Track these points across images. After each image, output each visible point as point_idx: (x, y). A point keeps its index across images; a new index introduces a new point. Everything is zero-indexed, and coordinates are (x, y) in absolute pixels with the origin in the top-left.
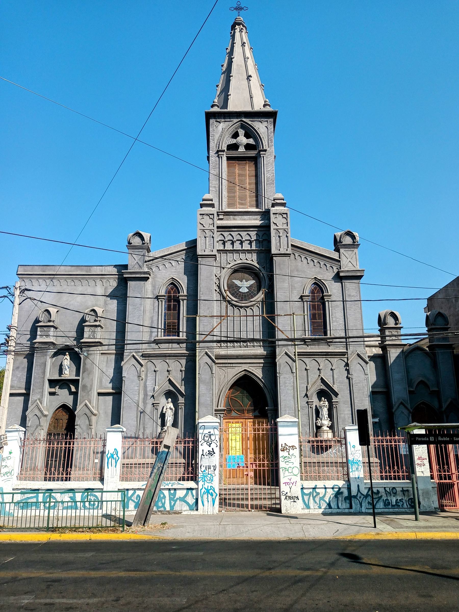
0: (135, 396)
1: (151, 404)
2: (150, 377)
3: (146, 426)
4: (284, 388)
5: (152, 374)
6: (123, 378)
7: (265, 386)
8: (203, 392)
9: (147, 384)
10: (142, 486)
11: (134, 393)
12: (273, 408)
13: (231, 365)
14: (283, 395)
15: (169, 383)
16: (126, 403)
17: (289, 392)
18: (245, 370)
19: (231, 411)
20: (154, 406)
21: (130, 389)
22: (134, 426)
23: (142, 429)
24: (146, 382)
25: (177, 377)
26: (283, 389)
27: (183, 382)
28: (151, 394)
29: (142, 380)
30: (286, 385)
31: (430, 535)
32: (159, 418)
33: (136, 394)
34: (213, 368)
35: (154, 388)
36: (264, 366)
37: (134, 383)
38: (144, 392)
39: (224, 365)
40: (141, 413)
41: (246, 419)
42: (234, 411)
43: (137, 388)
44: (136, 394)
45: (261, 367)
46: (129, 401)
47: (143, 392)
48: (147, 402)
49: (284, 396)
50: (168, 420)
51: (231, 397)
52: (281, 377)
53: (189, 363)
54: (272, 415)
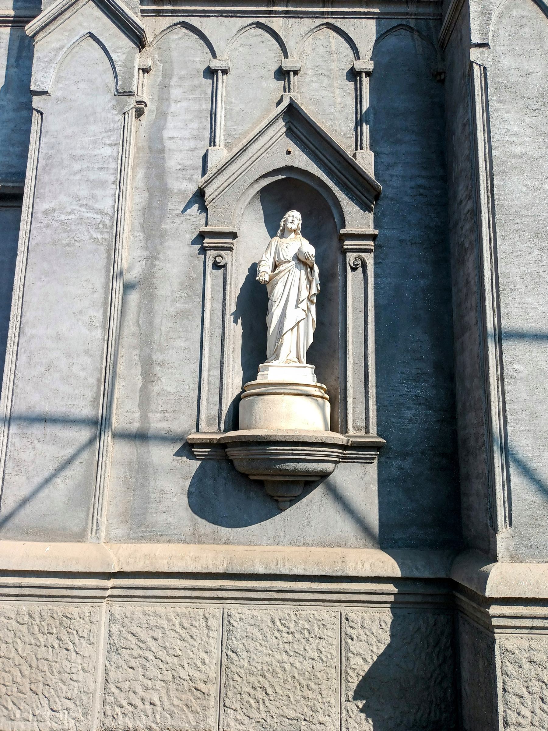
0: (99, 192)
1: (190, 237)
2: (184, 104)
3: (157, 357)
5: (194, 89)
6: (37, 102)
8: (517, 150)
9: (166, 134)
10: (368, 723)
11: (92, 176)
15: (290, 133)
16: (48, 226)
20: (203, 250)
21: (73, 158)
22: (87, 352)
23: (137, 371)
24: (163, 128)
25: (334, 104)
27: (366, 128)
28: (192, 188)
29: (139, 113)
32: (236, 315)
33: (102, 184)
35: (205, 158)
37: (93, 128)
38: (147, 178)
40: (128, 287)
43: (108, 151)
44: (102, 184)
46: (63, 217)
47: (141, 173)
48: (165, 226)
50: (289, 323)
53: (392, 41)
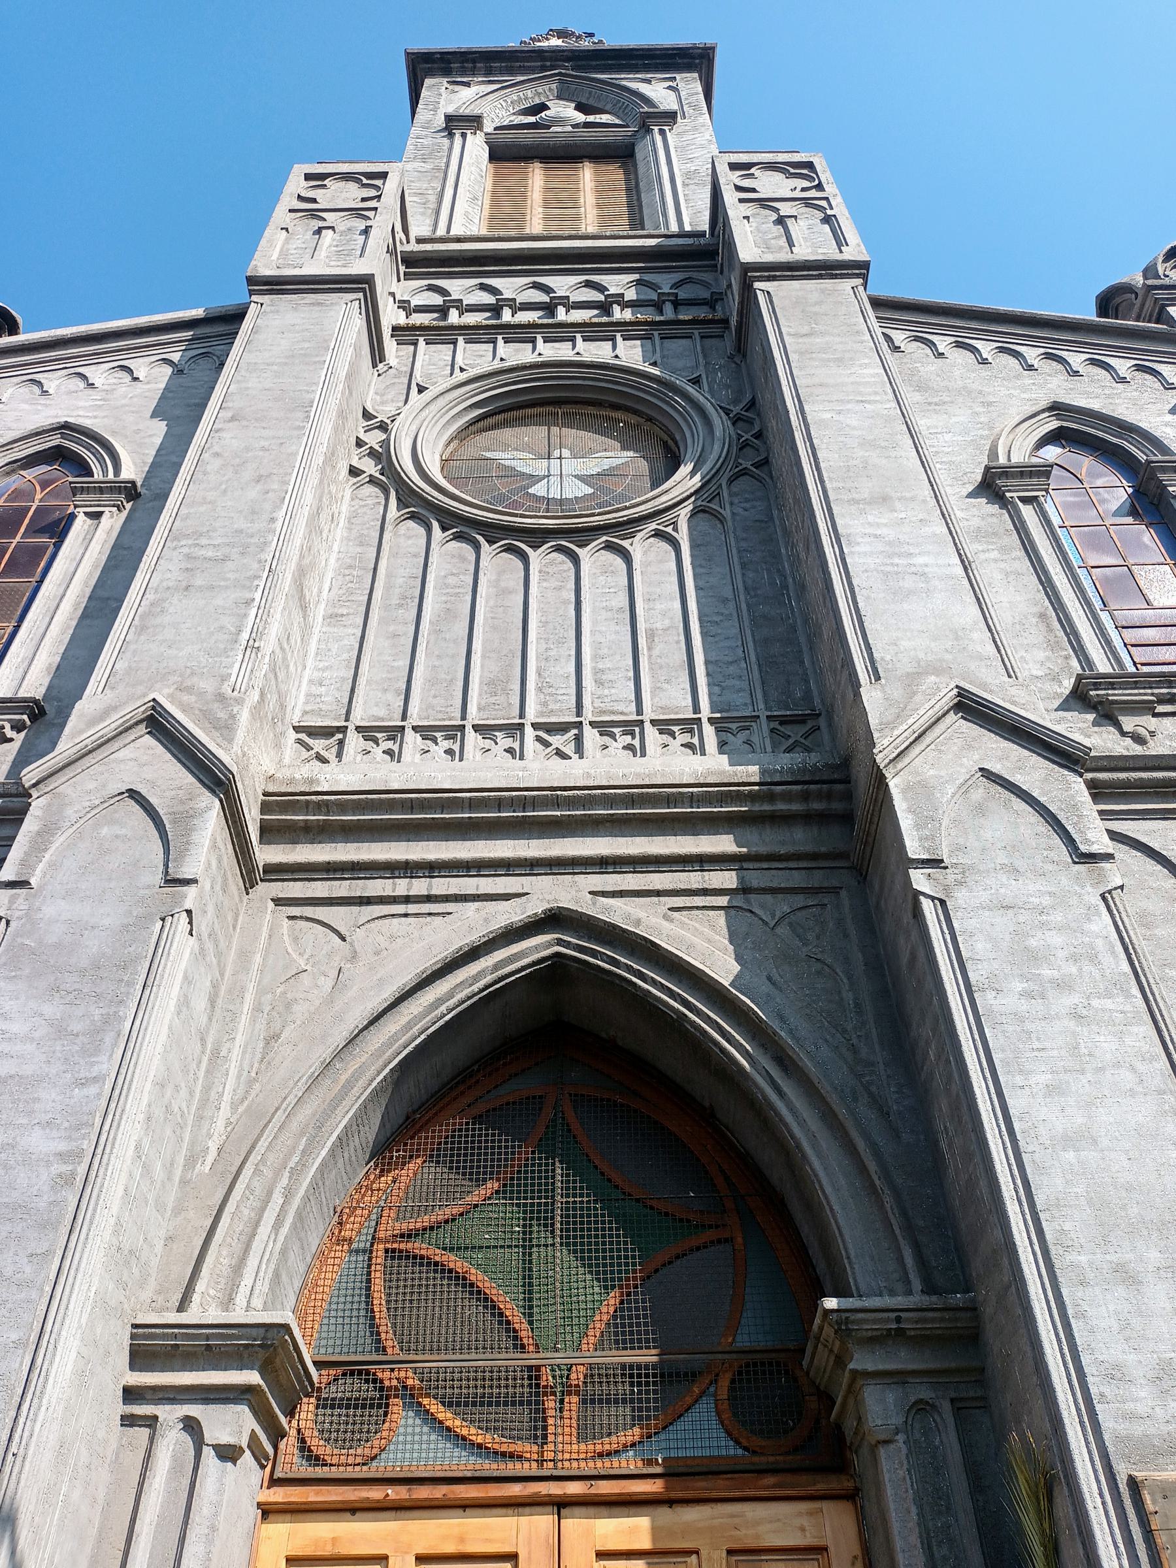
4: (1024, 1006)
7: (783, 1059)
12: (917, 1299)
13: (419, 886)
14: (1042, 1079)
17: (1106, 1045)
18: (554, 920)
19: (381, 1403)
26: (1019, 1018)
30: (1047, 972)
31: (157, 1479)
34: (188, 831)
36: (744, 890)
39: (342, 888)
41: (561, 1505)
42: (411, 1397)
45: (723, 901)
49: (1052, 1090)
51: (408, 1236)
52: (959, 900)
54: (921, 1408)
